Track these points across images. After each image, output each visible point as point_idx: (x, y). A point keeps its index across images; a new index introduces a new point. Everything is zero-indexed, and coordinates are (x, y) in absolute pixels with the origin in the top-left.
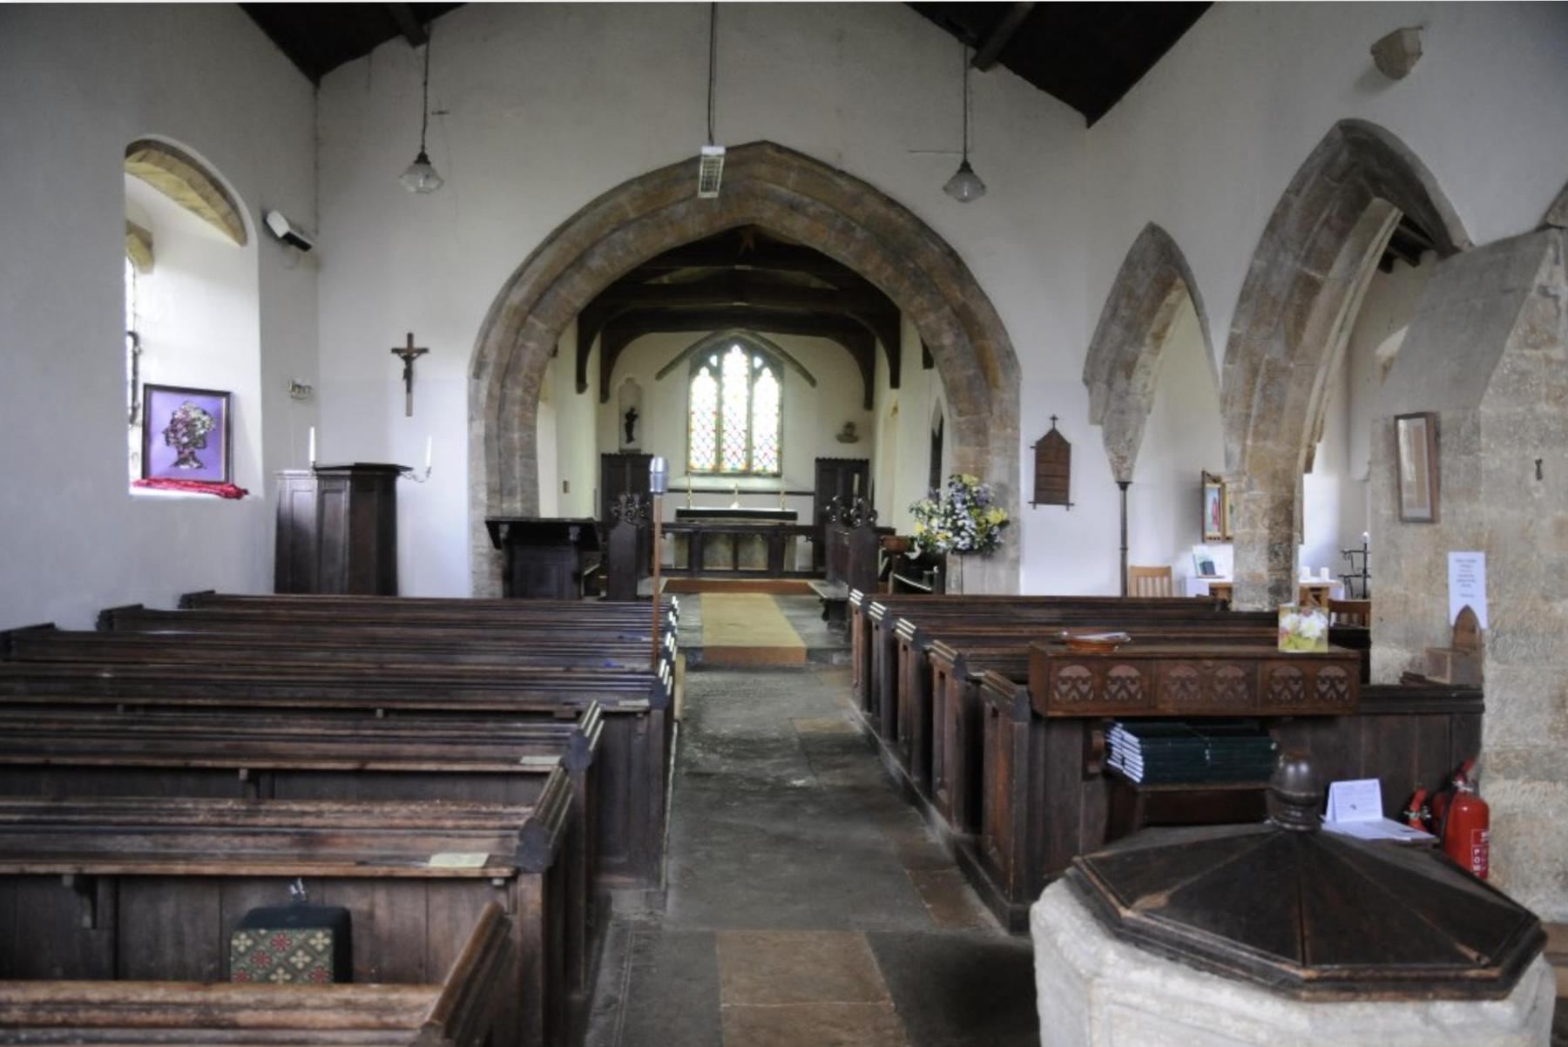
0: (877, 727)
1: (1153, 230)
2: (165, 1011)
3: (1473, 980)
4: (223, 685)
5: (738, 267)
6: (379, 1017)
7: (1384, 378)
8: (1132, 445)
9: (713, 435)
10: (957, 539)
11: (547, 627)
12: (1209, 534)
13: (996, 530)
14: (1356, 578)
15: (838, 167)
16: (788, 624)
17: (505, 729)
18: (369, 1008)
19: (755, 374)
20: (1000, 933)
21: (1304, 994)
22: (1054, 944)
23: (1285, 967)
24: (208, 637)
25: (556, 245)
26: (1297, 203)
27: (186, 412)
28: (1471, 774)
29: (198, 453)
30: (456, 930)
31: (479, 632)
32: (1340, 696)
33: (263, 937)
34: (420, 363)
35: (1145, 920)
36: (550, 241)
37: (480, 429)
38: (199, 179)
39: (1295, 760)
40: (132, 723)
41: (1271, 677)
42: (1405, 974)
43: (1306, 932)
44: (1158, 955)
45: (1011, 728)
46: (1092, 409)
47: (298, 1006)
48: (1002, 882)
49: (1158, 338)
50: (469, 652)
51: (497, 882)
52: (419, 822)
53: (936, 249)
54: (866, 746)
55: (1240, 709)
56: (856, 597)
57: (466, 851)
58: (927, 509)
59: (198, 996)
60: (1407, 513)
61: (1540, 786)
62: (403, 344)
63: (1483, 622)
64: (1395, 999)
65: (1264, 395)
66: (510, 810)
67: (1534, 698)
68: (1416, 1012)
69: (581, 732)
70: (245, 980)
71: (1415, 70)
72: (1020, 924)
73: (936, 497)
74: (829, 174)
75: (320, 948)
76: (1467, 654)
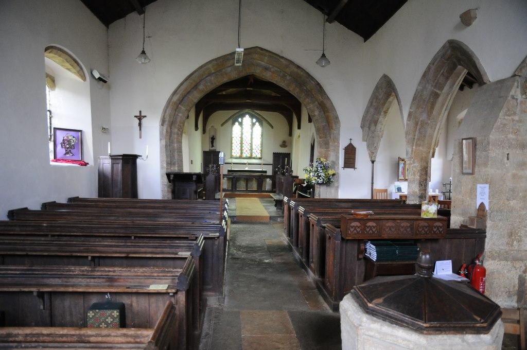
0: (292, 243)
1: (385, 76)
2: (67, 337)
3: (478, 327)
4: (82, 228)
5: (248, 89)
6: (134, 339)
7: (459, 126)
8: (376, 148)
9: (240, 145)
10: (318, 180)
11: (187, 209)
12: (400, 178)
13: (331, 177)
14: (447, 193)
15: (281, 55)
16: (264, 208)
17: (173, 243)
18: (131, 336)
19: (253, 124)
20: (330, 311)
21: (425, 332)
22: (347, 315)
23: (419, 323)
24: (77, 212)
25: (188, 81)
26: (433, 67)
27: (68, 137)
28: (481, 258)
29: (72, 150)
30: (158, 310)
31: (164, 211)
32: (440, 232)
33: (98, 312)
34: (144, 121)
35: (376, 307)
36: (186, 80)
37: (164, 142)
38: (69, 59)
39: (425, 254)
40: (53, 241)
41: (418, 226)
42: (457, 325)
43: (426, 311)
44: (379, 319)
45: (335, 243)
46: (363, 136)
47: (109, 336)
48: (330, 294)
49: (386, 112)
50: (161, 217)
51: (171, 294)
52: (146, 274)
53: (313, 82)
54: (288, 249)
55: (408, 237)
56: (286, 199)
57: (161, 284)
58: (309, 170)
59: (78, 332)
60: (465, 171)
61: (503, 262)
62: (138, 115)
63: (487, 208)
64: (453, 334)
65: (420, 134)
66: (175, 270)
67: (502, 233)
68: (460, 338)
69: (197, 244)
70: (92, 327)
71: (475, 23)
72: (336, 308)
73: (312, 166)
74: (278, 58)
75: (115, 316)
76: (481, 218)
